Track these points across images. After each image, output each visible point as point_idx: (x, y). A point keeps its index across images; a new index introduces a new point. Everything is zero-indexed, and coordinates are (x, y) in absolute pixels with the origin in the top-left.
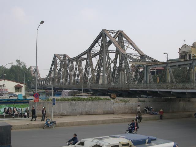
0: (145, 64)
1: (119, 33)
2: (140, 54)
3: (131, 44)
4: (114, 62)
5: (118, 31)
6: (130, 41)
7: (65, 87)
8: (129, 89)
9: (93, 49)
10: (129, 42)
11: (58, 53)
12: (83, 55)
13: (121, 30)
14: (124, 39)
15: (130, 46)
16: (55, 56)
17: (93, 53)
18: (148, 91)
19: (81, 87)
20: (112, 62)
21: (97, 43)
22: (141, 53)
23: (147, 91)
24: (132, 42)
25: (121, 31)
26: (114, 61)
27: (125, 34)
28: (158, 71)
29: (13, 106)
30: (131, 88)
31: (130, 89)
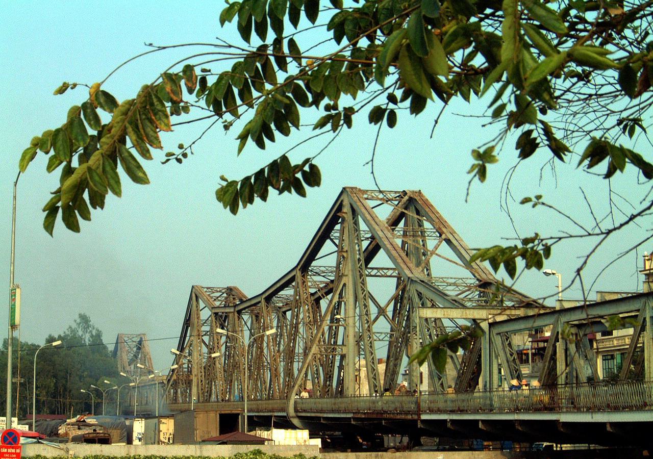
0: (484, 317)
1: (406, 198)
2: (478, 280)
3: (448, 241)
4: (390, 314)
5: (405, 193)
6: (444, 230)
7: (248, 411)
8: (419, 415)
9: (314, 263)
10: (441, 235)
11: (205, 282)
12: (282, 288)
13: (417, 189)
14: (427, 225)
15: (444, 249)
16: (195, 295)
17: (317, 278)
18: (483, 421)
19: (283, 410)
20: (382, 311)
21: (328, 241)
22: (484, 276)
23: (477, 421)
24: (453, 233)
25: (413, 192)
26: (391, 307)
27: (430, 206)
28: (453, 343)
29: (275, 448)
30: (425, 413)
31: (424, 417)
